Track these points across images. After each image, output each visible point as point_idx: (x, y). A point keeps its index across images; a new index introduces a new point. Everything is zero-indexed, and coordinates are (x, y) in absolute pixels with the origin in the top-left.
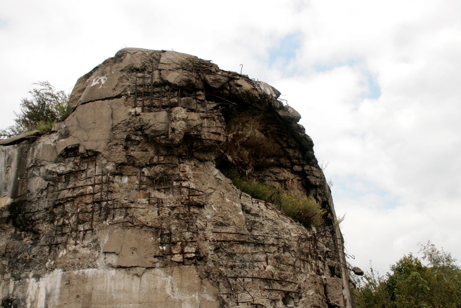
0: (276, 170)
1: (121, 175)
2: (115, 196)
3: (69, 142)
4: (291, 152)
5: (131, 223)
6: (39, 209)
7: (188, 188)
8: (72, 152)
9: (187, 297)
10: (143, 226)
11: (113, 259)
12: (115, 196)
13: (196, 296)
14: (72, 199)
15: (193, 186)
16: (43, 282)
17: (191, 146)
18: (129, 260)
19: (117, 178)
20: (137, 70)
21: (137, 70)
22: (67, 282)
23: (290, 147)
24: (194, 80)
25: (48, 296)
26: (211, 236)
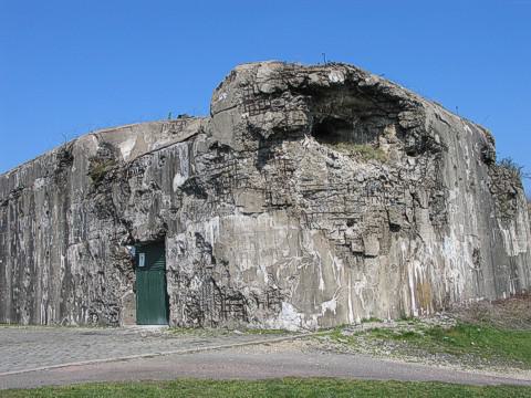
0: (376, 119)
1: (243, 158)
2: (240, 171)
3: (212, 140)
4: (382, 105)
5: (249, 186)
6: (143, 235)
7: (284, 159)
8: (214, 146)
9: (281, 228)
10: (256, 188)
11: (241, 209)
12: (240, 171)
13: (286, 227)
14: (220, 175)
15: (287, 158)
16: (211, 223)
17: (283, 133)
18: (250, 208)
19: (240, 161)
20: (244, 86)
21: (244, 86)
22: (222, 222)
23: (380, 102)
24: (280, 86)
25: (215, 230)
26: (298, 188)
